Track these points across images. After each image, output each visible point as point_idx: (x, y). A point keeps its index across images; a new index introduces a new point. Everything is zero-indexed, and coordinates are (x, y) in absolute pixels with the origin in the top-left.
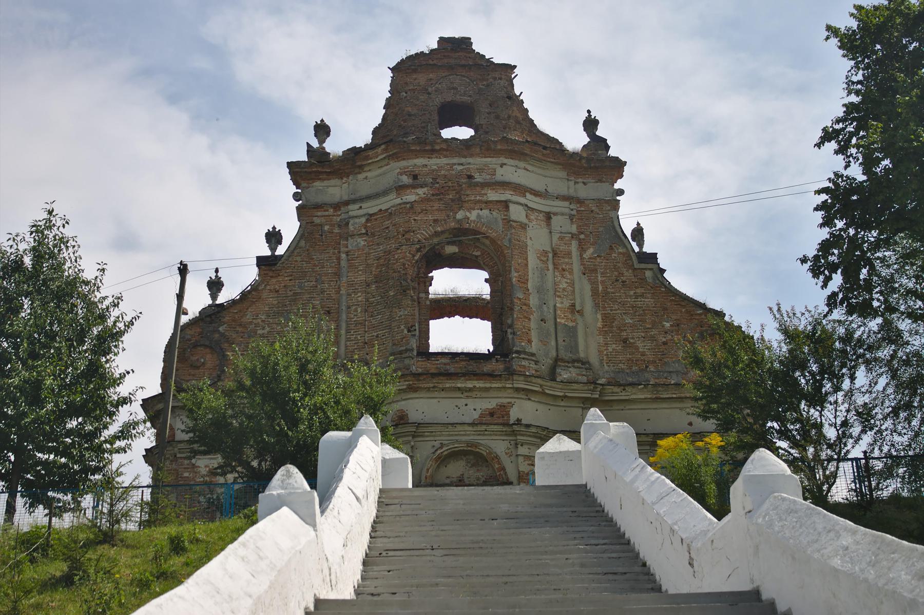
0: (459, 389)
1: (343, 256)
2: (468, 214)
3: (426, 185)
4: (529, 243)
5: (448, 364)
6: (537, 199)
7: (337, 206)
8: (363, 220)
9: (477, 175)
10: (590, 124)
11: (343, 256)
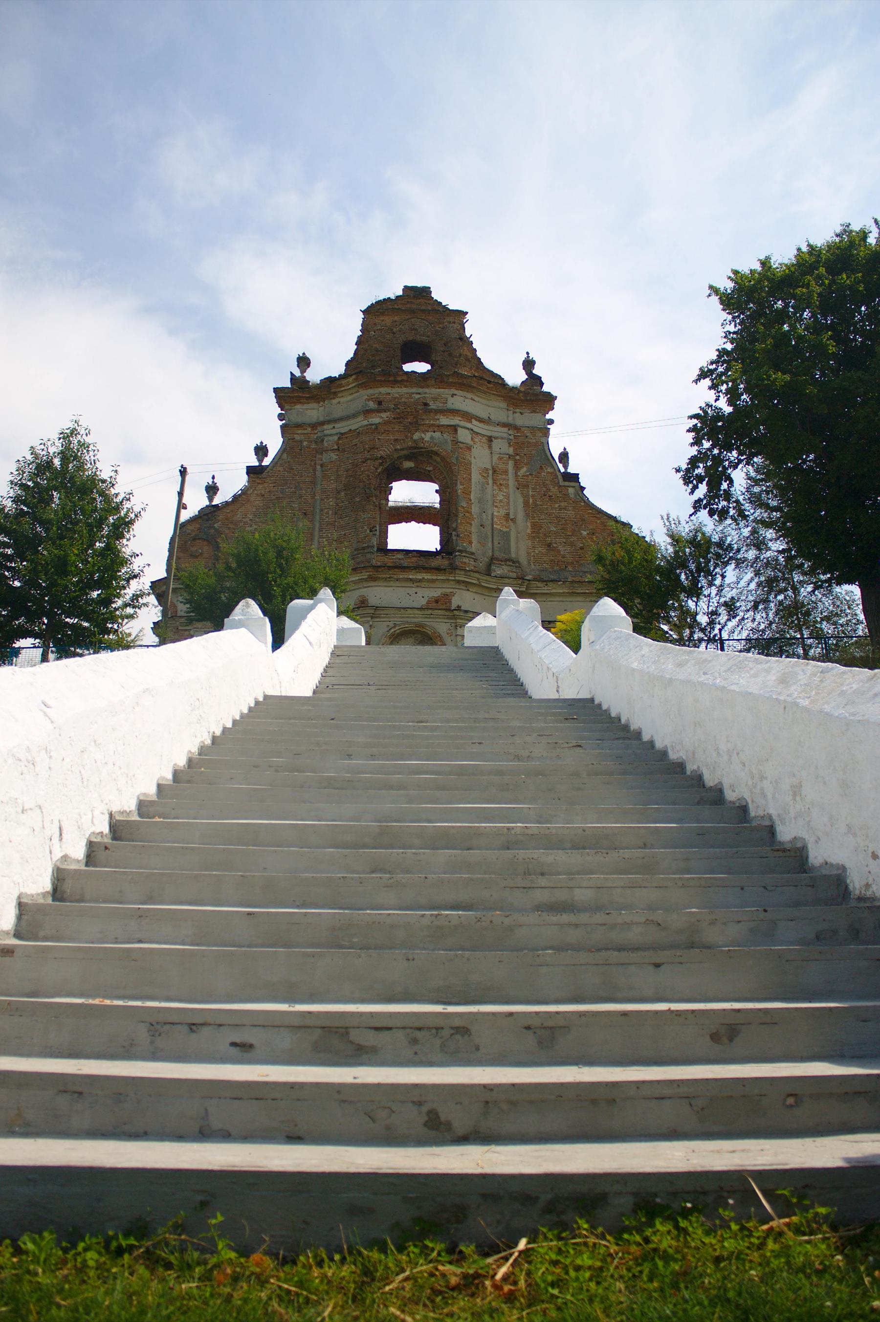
0: (411, 580)
1: (318, 467)
2: (423, 435)
3: (389, 410)
4: (473, 461)
5: (403, 559)
6: (481, 425)
7: (314, 426)
8: (336, 438)
9: (431, 403)
10: (529, 364)
11: (318, 467)
